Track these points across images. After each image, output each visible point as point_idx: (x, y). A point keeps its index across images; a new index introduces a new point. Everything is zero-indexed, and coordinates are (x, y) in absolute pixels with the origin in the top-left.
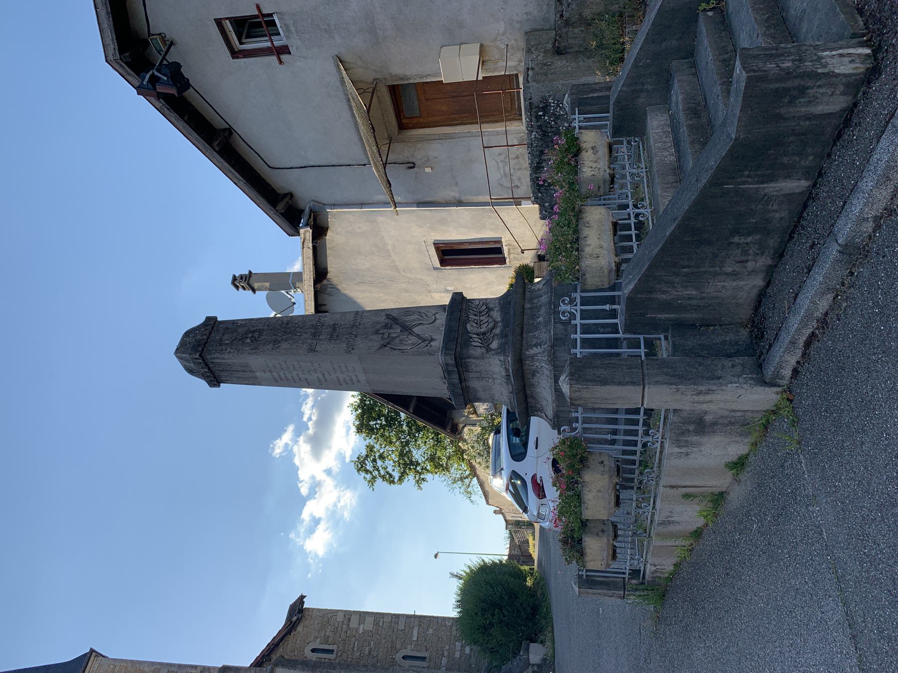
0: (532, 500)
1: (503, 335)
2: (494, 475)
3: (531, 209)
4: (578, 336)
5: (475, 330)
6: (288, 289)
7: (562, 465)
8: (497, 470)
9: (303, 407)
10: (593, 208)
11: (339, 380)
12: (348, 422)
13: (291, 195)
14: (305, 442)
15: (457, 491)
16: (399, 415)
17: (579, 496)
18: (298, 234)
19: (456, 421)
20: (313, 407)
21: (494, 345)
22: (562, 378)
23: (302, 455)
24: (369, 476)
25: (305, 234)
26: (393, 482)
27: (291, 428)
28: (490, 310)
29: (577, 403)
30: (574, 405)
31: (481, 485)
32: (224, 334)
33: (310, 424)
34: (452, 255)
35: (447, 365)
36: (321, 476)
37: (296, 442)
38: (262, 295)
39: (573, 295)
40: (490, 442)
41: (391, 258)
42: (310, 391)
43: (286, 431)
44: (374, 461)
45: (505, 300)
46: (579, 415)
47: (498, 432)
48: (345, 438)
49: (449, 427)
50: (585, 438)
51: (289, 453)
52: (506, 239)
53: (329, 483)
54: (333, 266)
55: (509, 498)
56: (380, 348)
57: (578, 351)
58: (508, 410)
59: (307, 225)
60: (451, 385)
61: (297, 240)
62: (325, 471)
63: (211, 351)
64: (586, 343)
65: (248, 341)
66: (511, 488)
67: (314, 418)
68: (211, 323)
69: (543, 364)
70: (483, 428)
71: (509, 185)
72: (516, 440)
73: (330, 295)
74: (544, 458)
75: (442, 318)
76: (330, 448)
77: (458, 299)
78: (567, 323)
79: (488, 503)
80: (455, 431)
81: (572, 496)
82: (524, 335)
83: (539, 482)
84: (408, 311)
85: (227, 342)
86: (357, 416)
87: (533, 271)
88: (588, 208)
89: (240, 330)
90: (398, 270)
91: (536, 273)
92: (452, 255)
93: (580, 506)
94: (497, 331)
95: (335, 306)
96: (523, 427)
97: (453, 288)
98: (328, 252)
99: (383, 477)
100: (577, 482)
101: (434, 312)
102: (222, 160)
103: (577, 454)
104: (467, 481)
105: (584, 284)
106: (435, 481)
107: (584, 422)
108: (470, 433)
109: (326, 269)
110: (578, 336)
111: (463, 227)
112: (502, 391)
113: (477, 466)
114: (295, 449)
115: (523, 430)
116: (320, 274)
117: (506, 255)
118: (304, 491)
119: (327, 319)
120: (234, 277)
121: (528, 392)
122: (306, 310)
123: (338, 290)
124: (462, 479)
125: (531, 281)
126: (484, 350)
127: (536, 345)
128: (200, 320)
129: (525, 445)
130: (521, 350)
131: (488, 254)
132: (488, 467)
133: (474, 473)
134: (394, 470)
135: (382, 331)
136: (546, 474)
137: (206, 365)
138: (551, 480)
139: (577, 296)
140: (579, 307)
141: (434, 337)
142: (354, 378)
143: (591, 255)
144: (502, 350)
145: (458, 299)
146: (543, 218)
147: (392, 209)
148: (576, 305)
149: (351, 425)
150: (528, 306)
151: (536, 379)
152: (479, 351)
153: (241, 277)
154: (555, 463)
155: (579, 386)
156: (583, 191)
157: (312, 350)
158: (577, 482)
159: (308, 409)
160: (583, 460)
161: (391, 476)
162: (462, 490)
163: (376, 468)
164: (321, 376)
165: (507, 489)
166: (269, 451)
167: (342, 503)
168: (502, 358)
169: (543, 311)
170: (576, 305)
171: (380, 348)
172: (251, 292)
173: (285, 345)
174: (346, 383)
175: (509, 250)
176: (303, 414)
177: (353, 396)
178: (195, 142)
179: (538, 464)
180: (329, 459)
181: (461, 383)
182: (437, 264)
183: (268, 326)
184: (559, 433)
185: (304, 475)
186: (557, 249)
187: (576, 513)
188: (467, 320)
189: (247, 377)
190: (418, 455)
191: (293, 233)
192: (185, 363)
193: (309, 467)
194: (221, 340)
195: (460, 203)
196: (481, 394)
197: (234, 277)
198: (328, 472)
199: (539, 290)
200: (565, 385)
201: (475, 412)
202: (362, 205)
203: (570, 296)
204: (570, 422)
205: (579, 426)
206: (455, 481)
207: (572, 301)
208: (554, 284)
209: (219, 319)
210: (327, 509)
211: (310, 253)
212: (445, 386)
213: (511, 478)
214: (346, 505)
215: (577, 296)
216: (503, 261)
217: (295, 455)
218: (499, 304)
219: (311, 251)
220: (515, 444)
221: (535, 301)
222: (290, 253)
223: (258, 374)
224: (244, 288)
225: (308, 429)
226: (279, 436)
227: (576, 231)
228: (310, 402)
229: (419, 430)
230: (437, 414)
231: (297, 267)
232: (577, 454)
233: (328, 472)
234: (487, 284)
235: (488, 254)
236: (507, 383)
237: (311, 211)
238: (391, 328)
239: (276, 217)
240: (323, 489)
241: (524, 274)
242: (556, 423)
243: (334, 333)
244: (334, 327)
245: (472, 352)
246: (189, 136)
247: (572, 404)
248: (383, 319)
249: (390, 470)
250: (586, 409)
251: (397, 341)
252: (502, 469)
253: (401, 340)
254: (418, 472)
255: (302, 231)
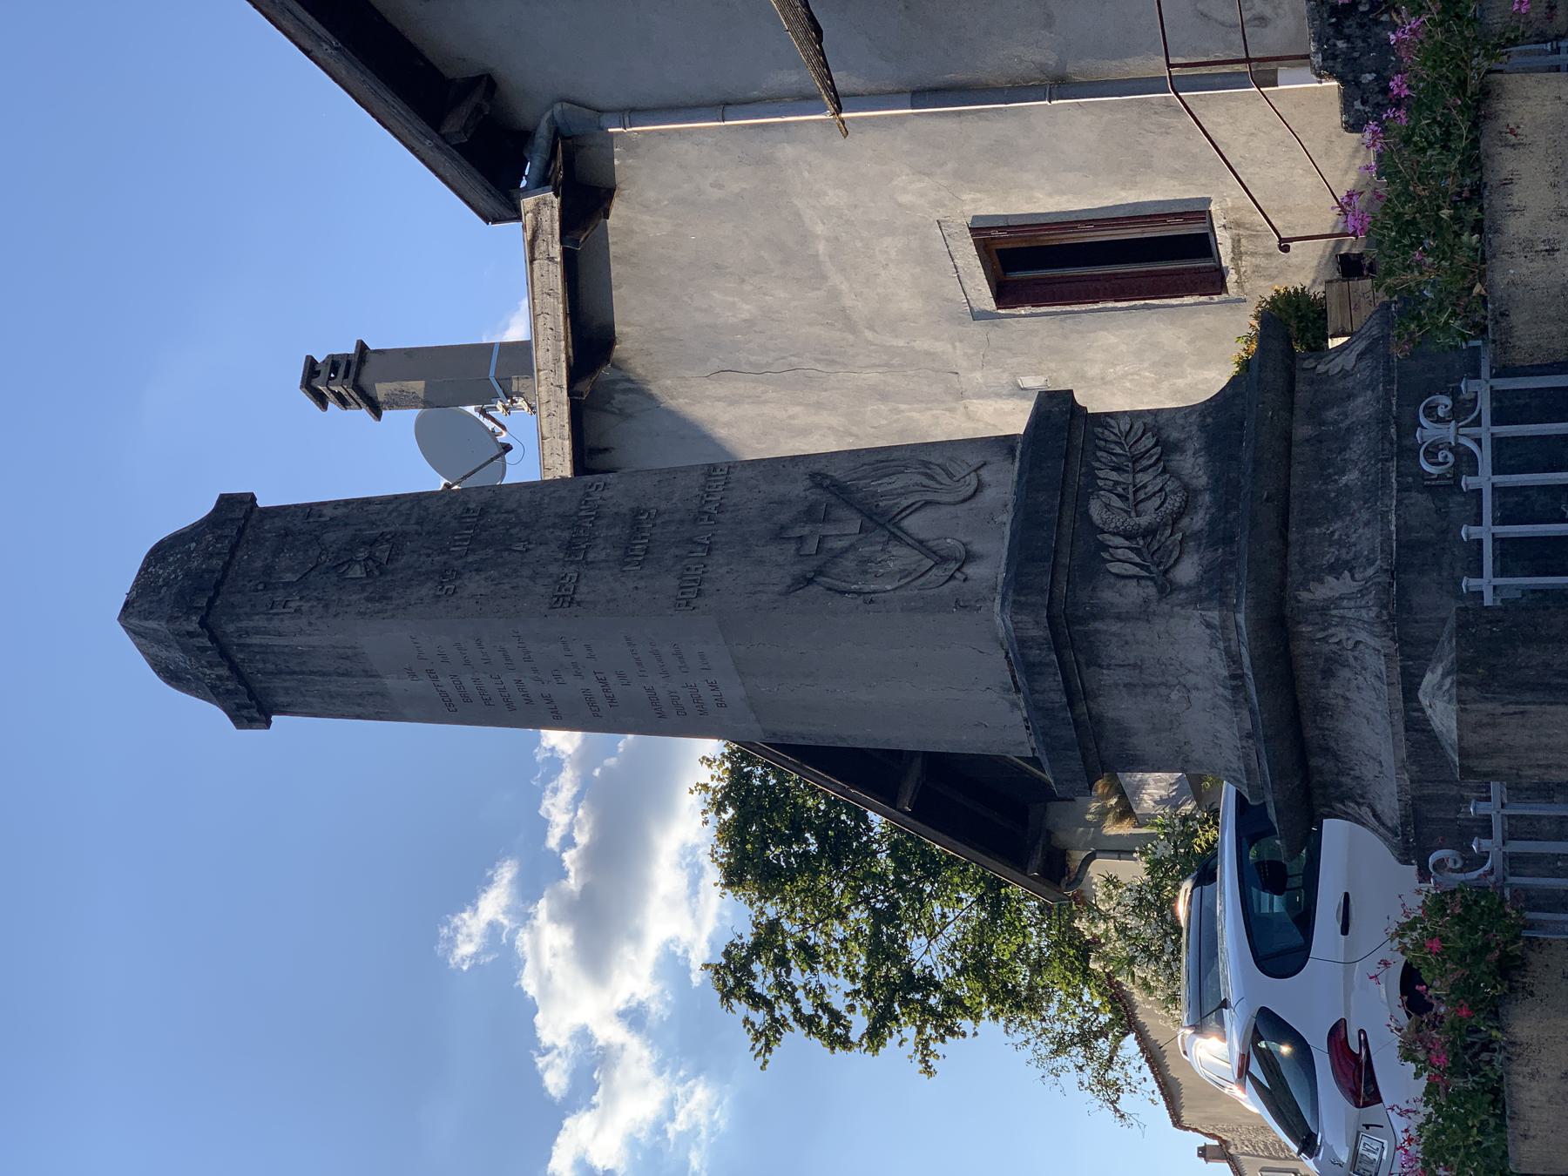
0: (1333, 1111)
1: (1219, 536)
2: (1199, 1027)
3: (1312, 94)
4: (1486, 532)
5: (1118, 521)
6: (484, 399)
7: (1436, 988)
8: (1206, 1011)
9: (546, 803)
10: (1530, 80)
11: (654, 700)
12: (695, 848)
13: (487, 83)
14: (553, 918)
15: (1070, 1078)
16: (865, 819)
17: (1496, 1095)
18: (513, 213)
19: (1062, 837)
20: (577, 800)
21: (1187, 571)
22: (1430, 679)
23: (547, 961)
24: (760, 1017)
25: (537, 212)
26: (845, 1043)
27: (506, 873)
28: (1168, 448)
29: (1487, 765)
30: (1474, 773)
31: (1154, 1057)
32: (277, 553)
33: (569, 857)
34: (1034, 266)
35: (1022, 642)
36: (610, 1033)
37: (524, 918)
38: (401, 422)
39: (1467, 387)
40: (1182, 909)
41: (838, 294)
42: (562, 741)
43: (490, 882)
44: (781, 961)
45: (1220, 415)
46: (1491, 809)
47: (1206, 875)
48: (687, 903)
49: (1037, 860)
50: (1516, 892)
51: (502, 957)
52: (1225, 204)
53: (637, 1054)
54: (633, 318)
55: (1250, 1102)
56: (789, 591)
57: (1487, 585)
58: (1239, 796)
59: (542, 182)
60: (1039, 716)
61: (511, 234)
62: (621, 1015)
63: (242, 607)
64: (1512, 555)
65: (357, 572)
66: (1255, 1068)
67: (582, 838)
68: (236, 511)
69: (1362, 636)
70: (1155, 866)
71: (1232, 16)
72: (1273, 904)
73: (624, 415)
74: (1372, 965)
75: (1002, 483)
76: (637, 937)
77: (1058, 414)
78: (1446, 489)
79: (1177, 1122)
80: (1058, 874)
81: (1470, 1094)
82: (1293, 536)
83: (1354, 1046)
84: (884, 460)
85: (289, 577)
86: (723, 829)
87: (1322, 314)
88: (1511, 81)
89: (329, 537)
90: (850, 326)
91: (1334, 318)
92: (1034, 266)
93: (1501, 1127)
94: (1198, 521)
95: (641, 453)
96: (1294, 854)
97: (1035, 382)
98: (616, 269)
99: (809, 1023)
100: (1487, 1046)
101: (975, 461)
102: (557, 225)
103: (1487, 947)
104: (1103, 1045)
105: (1504, 345)
106: (990, 1046)
107: (1510, 836)
108: (1114, 878)
109: (610, 329)
110: (1486, 532)
111: (1070, 168)
112: (1218, 726)
113: (1138, 996)
114: (524, 940)
115: (1295, 867)
116: (590, 343)
117: (1226, 262)
118: (555, 1081)
119: (615, 493)
120: (311, 363)
121: (1311, 733)
122: (544, 468)
123: (650, 397)
124: (1086, 1038)
125: (1317, 349)
126: (1152, 591)
127: (1335, 569)
128: (203, 508)
129: (1304, 919)
130: (1283, 586)
131: (1160, 257)
132: (1174, 998)
133: (1126, 1019)
134: (852, 1008)
135: (798, 531)
136: (1379, 1018)
137: (224, 654)
138: (1396, 1039)
139: (1481, 390)
140: (1486, 430)
141: (976, 547)
142: (706, 694)
143: (1528, 245)
144: (1213, 588)
145: (1058, 414)
146: (1354, 126)
147: (826, 116)
148: (1477, 422)
149: (706, 861)
150: (1302, 431)
151: (1336, 687)
152: (1133, 594)
153: (334, 363)
154: (1410, 978)
155: (1489, 707)
156: (1496, 20)
157: (564, 599)
158: (1487, 1046)
159: (560, 810)
160: (1510, 969)
161: (836, 1017)
162: (1088, 1075)
163: (785, 990)
164: (596, 689)
165: (1244, 1071)
166: (440, 948)
167: (680, 1124)
168: (1214, 616)
169: (1358, 447)
170: (1477, 422)
171: (789, 591)
172: (364, 414)
173: (474, 584)
174: (682, 711)
175: (1236, 242)
176: (544, 825)
177: (708, 761)
178: (308, 45)
179: (1350, 987)
180: (635, 978)
181: (1071, 704)
182: (983, 295)
183: (420, 523)
184: (1424, 875)
185: (554, 1027)
186: (1406, 226)
187: (1486, 1153)
188: (1091, 486)
189: (355, 693)
190: (925, 954)
191: (501, 210)
192: (155, 649)
193: (573, 1005)
194: (268, 570)
195: (1060, 86)
196: (1143, 743)
197: (311, 363)
198: (634, 1017)
199: (1345, 374)
200: (1440, 705)
201: (1126, 811)
202: (723, 106)
203: (1455, 394)
204: (1461, 835)
205: (1491, 846)
206: (1061, 1046)
207: (1462, 410)
208: (1397, 354)
209: (261, 503)
210: (632, 1142)
211: (553, 276)
212: (1020, 715)
213: (1256, 1036)
214: (694, 1132)
215: (1481, 390)
216: (1213, 281)
217: (521, 963)
218: (1203, 428)
219: (557, 271)
220: (1268, 920)
221: (1331, 414)
222: (483, 280)
223: (390, 682)
224: (343, 402)
225: (564, 875)
226: (469, 899)
227: (1473, 162)
228: (567, 784)
229: (932, 868)
230: (997, 817)
231: (517, 331)
232: (1487, 947)
233: (634, 1017)
234: (1155, 363)
235: (1160, 257)
236: (1234, 703)
237: (557, 133)
238: (826, 519)
239: (441, 159)
240: (618, 1074)
241: (1290, 325)
242: (1413, 841)
243: (637, 538)
244: (636, 520)
245: (1108, 595)
246: (391, 122)
247: (1466, 771)
248: (799, 489)
249: (838, 1002)
250: (1517, 791)
251: (849, 563)
252: (1225, 1004)
253: (865, 561)
254: (932, 1011)
255: (527, 203)
